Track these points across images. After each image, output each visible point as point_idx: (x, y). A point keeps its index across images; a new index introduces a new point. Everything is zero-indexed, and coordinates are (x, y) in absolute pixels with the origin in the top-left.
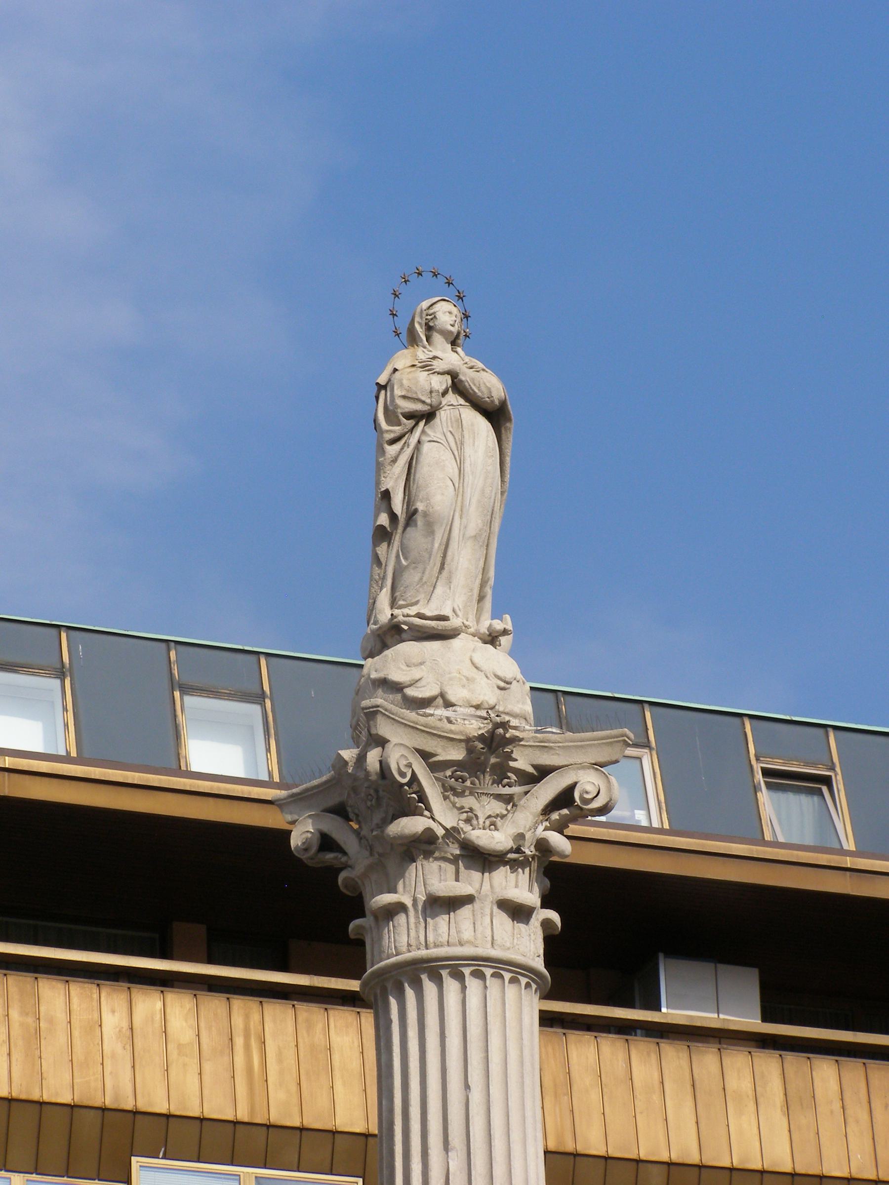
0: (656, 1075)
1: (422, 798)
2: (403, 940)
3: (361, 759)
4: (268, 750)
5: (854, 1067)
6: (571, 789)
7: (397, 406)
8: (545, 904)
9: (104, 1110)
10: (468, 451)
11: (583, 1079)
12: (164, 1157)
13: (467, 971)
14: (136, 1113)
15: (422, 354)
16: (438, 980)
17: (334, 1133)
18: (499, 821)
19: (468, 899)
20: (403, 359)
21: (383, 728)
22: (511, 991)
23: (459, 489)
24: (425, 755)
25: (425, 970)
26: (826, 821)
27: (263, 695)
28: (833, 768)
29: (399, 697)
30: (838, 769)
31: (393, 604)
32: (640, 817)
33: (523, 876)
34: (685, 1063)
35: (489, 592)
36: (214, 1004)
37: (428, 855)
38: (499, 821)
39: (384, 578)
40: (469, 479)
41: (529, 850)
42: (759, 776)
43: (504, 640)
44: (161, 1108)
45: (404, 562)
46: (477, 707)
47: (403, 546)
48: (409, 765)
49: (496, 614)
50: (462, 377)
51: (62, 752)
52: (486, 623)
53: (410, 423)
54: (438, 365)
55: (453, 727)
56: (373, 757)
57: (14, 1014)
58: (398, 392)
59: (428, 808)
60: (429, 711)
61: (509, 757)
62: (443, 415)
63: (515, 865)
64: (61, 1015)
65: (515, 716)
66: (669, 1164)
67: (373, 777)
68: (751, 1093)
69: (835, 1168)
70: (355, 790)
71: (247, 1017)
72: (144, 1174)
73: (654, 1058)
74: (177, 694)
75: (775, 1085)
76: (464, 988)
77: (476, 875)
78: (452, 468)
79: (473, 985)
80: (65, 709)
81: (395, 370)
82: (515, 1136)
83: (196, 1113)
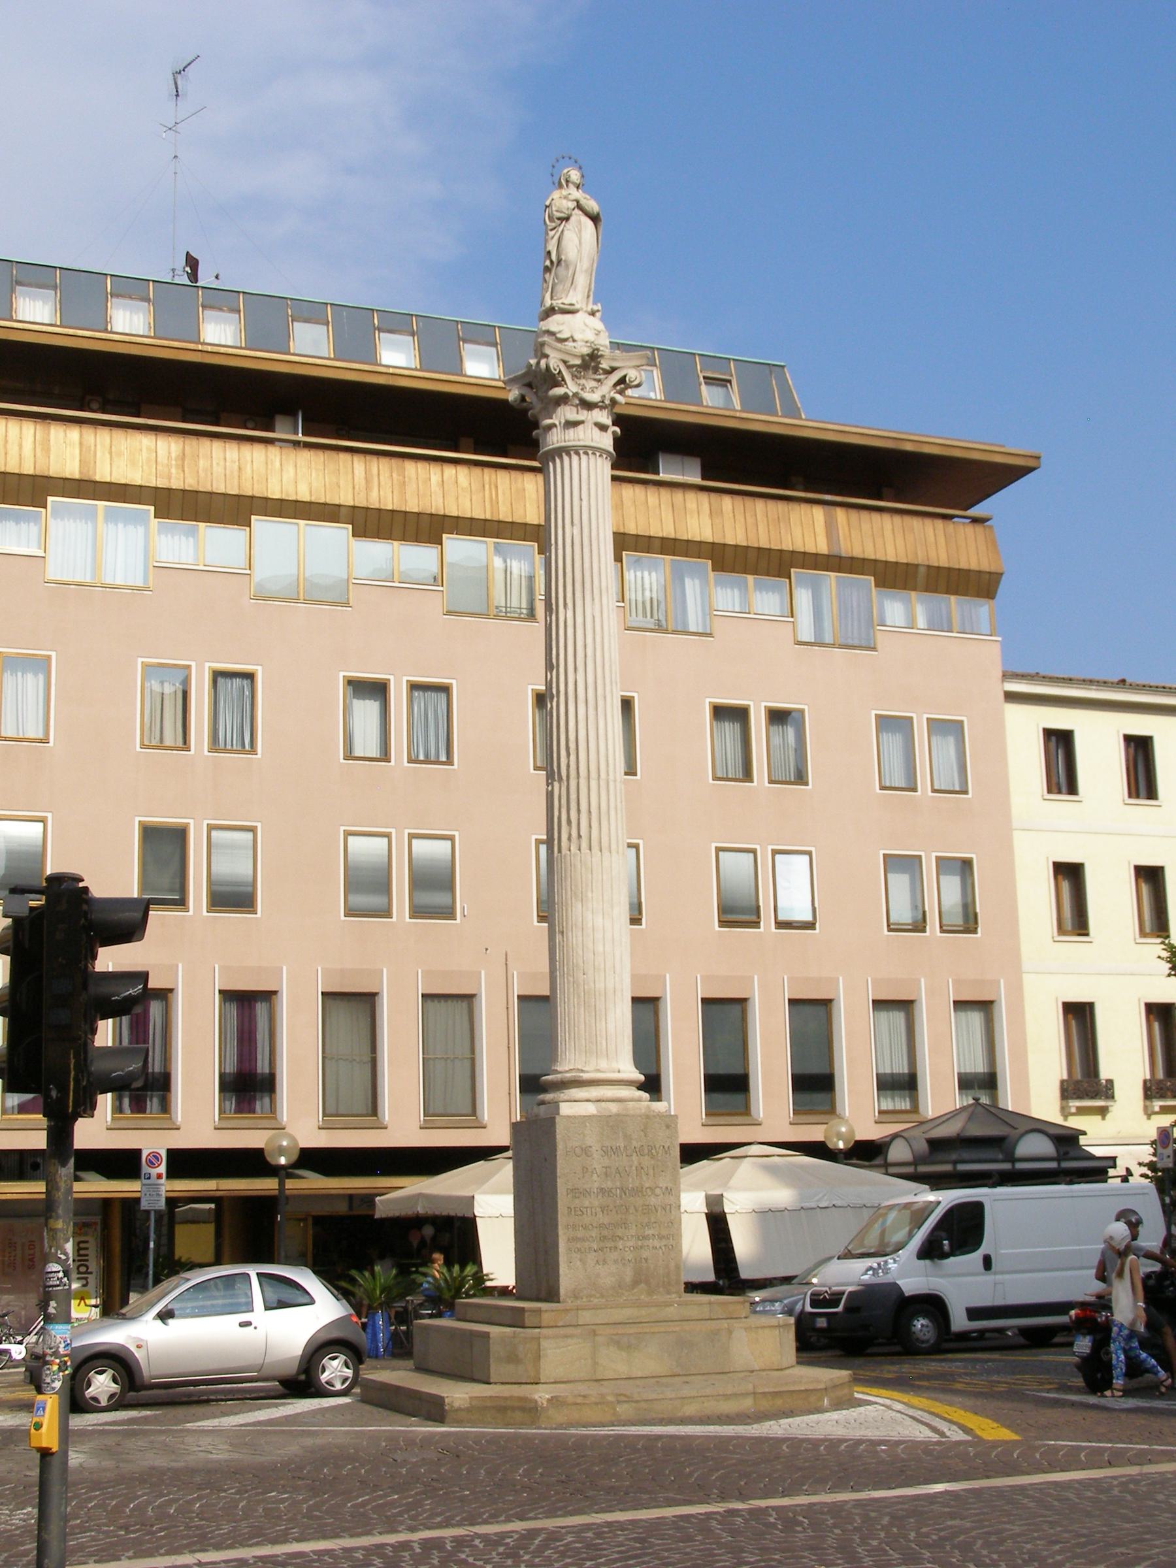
0: (657, 501)
1: (563, 380)
2: (555, 439)
3: (538, 363)
4: (499, 366)
5: (739, 500)
6: (625, 377)
7: (553, 215)
8: (614, 424)
9: (432, 515)
10: (583, 233)
11: (627, 502)
12: (457, 534)
13: (581, 452)
14: (445, 516)
15: (564, 192)
16: (569, 455)
17: (526, 524)
18: (595, 390)
19: (582, 422)
20: (556, 195)
21: (547, 350)
22: (599, 460)
23: (579, 251)
24: (565, 362)
25: (564, 451)
26: (728, 398)
27: (497, 344)
28: (732, 376)
29: (554, 338)
30: (734, 376)
31: (552, 298)
32: (652, 395)
33: (605, 412)
34: (669, 496)
35: (591, 293)
36: (477, 471)
37: (566, 403)
38: (595, 390)
39: (548, 288)
40: (584, 245)
41: (607, 402)
42: (702, 379)
43: (598, 315)
44: (455, 514)
45: (556, 281)
46: (587, 342)
47: (555, 273)
48: (558, 366)
49: (595, 303)
50: (581, 202)
51: (414, 367)
52: (590, 307)
53: (559, 222)
54: (571, 197)
55: (576, 350)
56: (543, 363)
57: (394, 475)
58: (554, 209)
59: (566, 384)
60: (566, 343)
61: (599, 363)
62: (573, 219)
63: (602, 408)
64: (413, 476)
65: (602, 346)
66: (663, 538)
67: (543, 371)
68: (696, 510)
69: (730, 541)
70: (536, 377)
71: (490, 477)
72: (448, 541)
73: (657, 494)
74: (461, 343)
75: (706, 506)
76: (580, 459)
77: (585, 412)
78: (576, 241)
79: (584, 457)
80: (415, 349)
81: (553, 199)
82: (601, 520)
83: (469, 516)
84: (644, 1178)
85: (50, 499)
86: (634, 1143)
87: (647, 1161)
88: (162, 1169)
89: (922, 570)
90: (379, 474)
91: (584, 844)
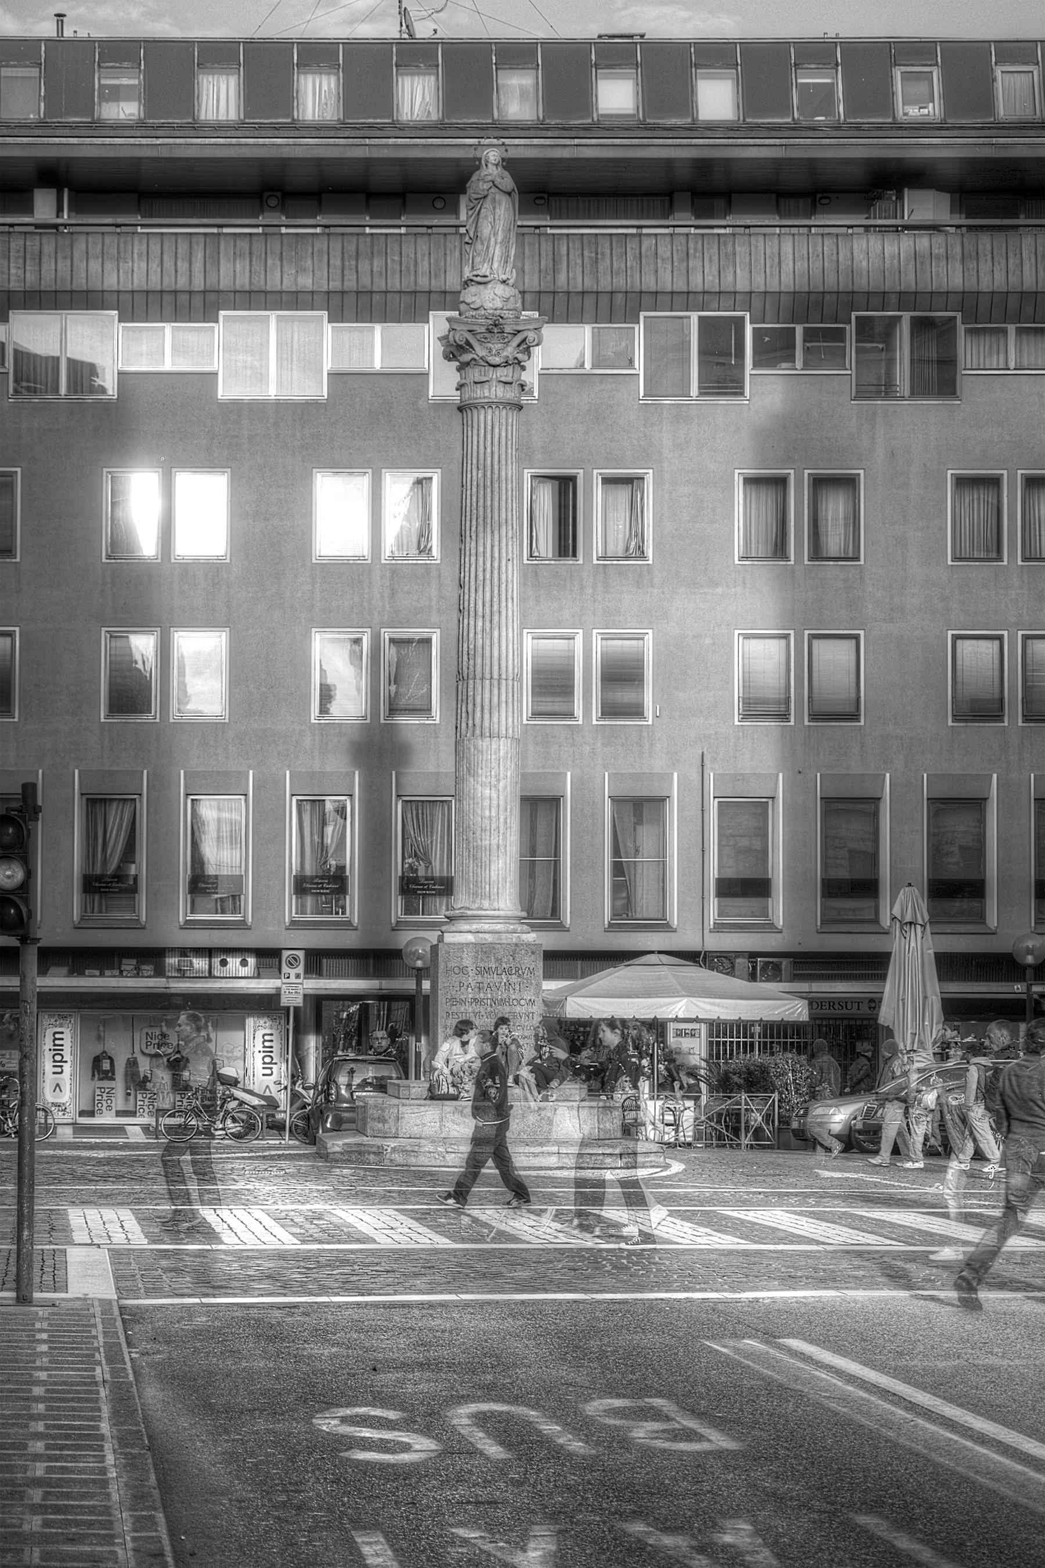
84: (512, 992)
85: (222, 313)
86: (504, 965)
87: (514, 979)
88: (300, 970)
90: (568, 254)
91: (478, 732)
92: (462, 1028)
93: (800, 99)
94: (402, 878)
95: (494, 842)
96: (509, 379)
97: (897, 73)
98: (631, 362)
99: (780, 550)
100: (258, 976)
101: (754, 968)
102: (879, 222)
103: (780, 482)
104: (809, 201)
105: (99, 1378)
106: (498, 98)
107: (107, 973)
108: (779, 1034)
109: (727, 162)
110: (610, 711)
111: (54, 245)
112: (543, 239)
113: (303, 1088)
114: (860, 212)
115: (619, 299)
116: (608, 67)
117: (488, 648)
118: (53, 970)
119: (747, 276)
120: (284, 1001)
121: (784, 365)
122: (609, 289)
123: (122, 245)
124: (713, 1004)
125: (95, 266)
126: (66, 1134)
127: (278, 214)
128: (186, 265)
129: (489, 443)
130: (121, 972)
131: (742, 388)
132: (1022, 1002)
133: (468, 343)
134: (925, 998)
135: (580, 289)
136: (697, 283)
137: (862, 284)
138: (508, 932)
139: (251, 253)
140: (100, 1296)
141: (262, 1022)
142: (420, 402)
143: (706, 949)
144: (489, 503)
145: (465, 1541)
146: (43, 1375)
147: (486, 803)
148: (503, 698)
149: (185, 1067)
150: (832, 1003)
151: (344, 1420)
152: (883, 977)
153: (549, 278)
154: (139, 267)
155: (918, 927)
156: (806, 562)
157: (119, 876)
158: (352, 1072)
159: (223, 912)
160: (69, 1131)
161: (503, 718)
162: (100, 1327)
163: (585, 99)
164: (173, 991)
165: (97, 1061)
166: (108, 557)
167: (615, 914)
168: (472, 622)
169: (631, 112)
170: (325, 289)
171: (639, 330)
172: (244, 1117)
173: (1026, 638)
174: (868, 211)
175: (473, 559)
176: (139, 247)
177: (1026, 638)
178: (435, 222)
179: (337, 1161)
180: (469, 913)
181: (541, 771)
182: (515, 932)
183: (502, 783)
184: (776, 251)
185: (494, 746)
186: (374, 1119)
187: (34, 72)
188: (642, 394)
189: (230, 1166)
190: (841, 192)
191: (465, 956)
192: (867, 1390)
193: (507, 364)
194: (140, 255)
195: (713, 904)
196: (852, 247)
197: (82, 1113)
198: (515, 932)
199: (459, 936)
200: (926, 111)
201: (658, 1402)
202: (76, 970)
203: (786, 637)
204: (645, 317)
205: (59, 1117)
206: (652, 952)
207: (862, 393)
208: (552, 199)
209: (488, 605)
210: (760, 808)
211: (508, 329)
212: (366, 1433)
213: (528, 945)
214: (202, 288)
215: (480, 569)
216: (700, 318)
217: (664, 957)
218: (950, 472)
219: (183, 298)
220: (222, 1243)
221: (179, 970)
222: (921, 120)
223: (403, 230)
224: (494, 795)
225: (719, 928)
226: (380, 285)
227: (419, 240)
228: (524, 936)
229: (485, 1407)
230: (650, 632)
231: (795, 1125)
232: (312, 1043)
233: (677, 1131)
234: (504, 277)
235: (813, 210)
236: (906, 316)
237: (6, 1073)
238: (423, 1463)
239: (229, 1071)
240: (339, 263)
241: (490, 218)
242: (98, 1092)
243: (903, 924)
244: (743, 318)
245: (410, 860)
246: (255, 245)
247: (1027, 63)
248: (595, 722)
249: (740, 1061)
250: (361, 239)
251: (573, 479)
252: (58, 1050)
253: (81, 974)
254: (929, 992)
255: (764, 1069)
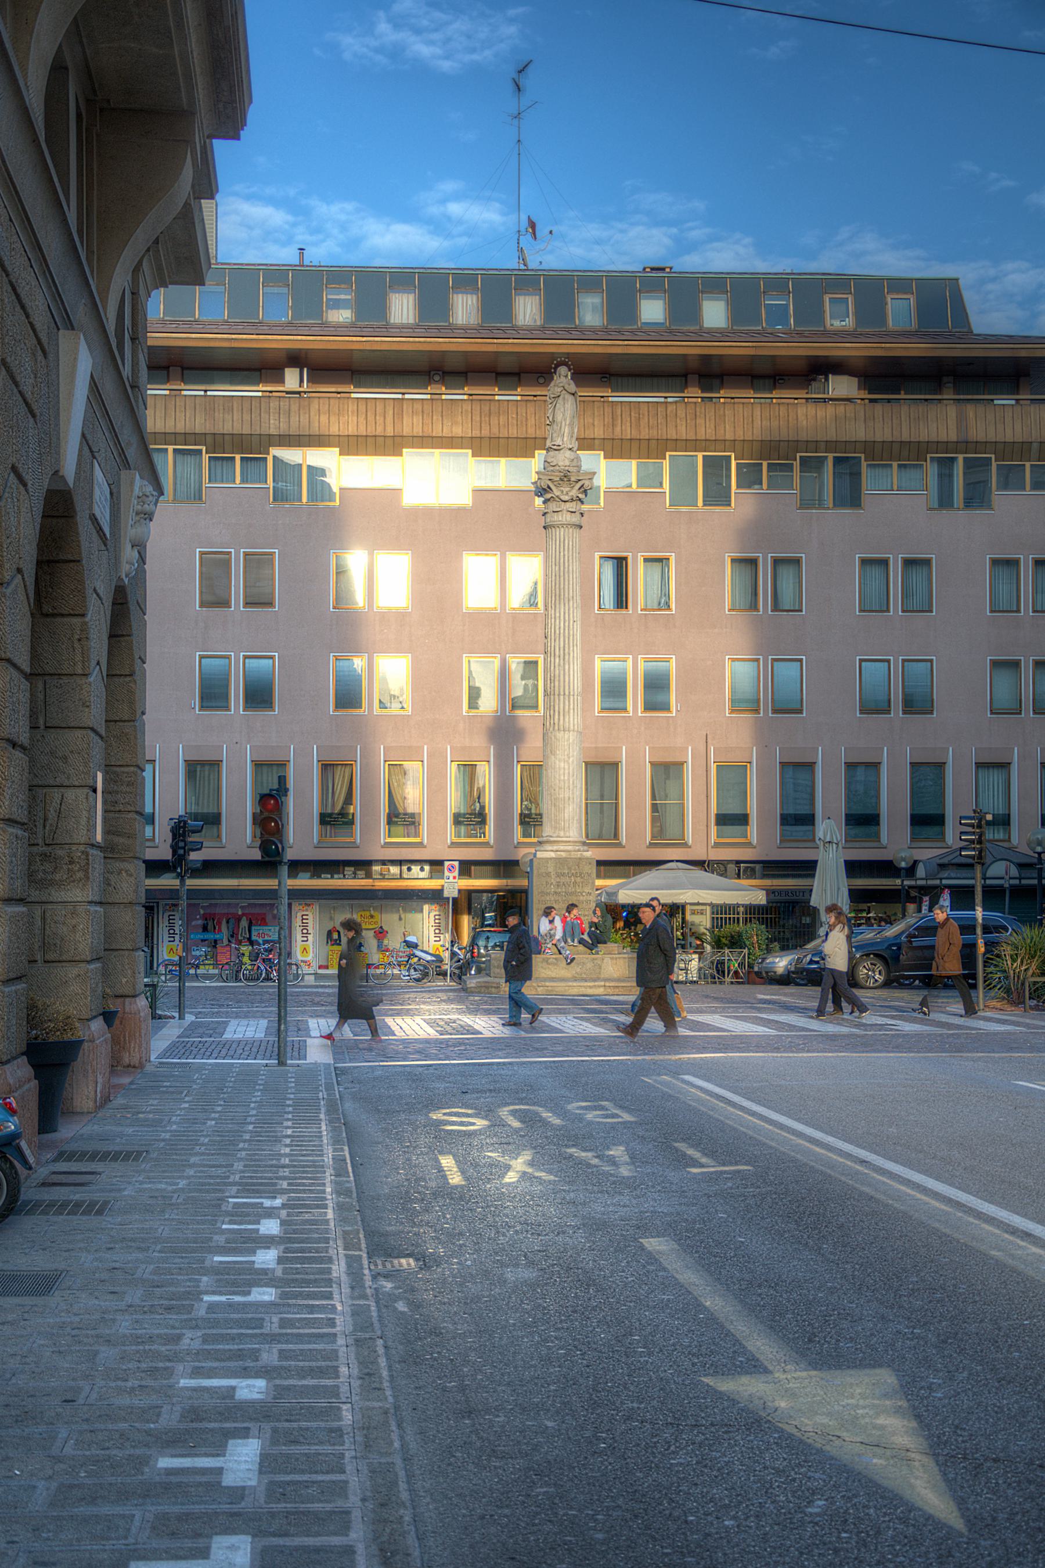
87: (578, 880)
88: (456, 873)
89: (1035, 446)
91: (556, 728)
92: (547, 912)
93: (766, 313)
94: (521, 814)
95: (567, 796)
96: (573, 510)
97: (827, 298)
98: (661, 484)
99: (754, 606)
100: (431, 878)
101: (739, 870)
102: (814, 396)
103: (753, 562)
104: (772, 381)
105: (321, 1097)
106: (579, 312)
107: (336, 876)
108: (759, 912)
109: (721, 357)
110: (649, 707)
111: (297, 405)
112: (606, 404)
113: (459, 949)
114: (802, 388)
115: (653, 444)
116: (647, 292)
117: (562, 676)
118: (301, 875)
119: (732, 429)
120: (446, 894)
121: (756, 487)
122: (647, 437)
123: (341, 406)
124: (708, 894)
125: (324, 419)
126: (310, 980)
127: (440, 386)
128: (382, 419)
129: (562, 549)
130: (344, 876)
131: (730, 501)
132: (899, 890)
133: (549, 487)
134: (839, 889)
135: (629, 437)
136: (701, 435)
137: (803, 437)
138: (575, 851)
139: (423, 412)
140: (324, 1062)
141: (433, 907)
142: (530, 509)
143: (710, 859)
144: (562, 586)
145: (489, 1157)
146: (292, 1096)
147: (562, 772)
148: (572, 707)
149: (385, 937)
150: (780, 892)
151: (444, 1114)
152: (813, 876)
153: (610, 430)
154: (352, 420)
155: (834, 845)
156: (770, 613)
157: (343, 814)
158: (488, 938)
159: (408, 837)
160: (312, 978)
161: (572, 719)
162: (323, 1076)
163: (632, 311)
164: (377, 888)
165: (329, 934)
166: (334, 608)
167: (653, 837)
168: (552, 660)
169: (662, 321)
170: (470, 435)
171: (666, 464)
172: (422, 968)
173: (904, 661)
174: (807, 388)
175: (553, 620)
176: (352, 407)
177: (904, 661)
178: (539, 393)
179: (472, 992)
180: (552, 839)
181: (606, 745)
182: (579, 850)
183: (571, 759)
184: (750, 414)
185: (566, 736)
186: (494, 967)
187: (285, 290)
188: (668, 505)
189: (408, 996)
190: (792, 375)
191: (549, 865)
192: (711, 1096)
193: (572, 500)
194: (353, 412)
195: (713, 829)
196: (797, 412)
197: (320, 967)
198: (579, 850)
199: (546, 854)
200: (843, 323)
201: (603, 1103)
202: (316, 875)
203: (758, 660)
204: (670, 456)
205: (306, 969)
206: (672, 861)
207: (805, 504)
208: (612, 378)
209: (562, 649)
210: (741, 770)
211: (573, 479)
212: (454, 1119)
213: (587, 859)
214: (392, 434)
215: (557, 627)
216: (703, 456)
217: (679, 864)
218: (857, 556)
219: (380, 440)
220: (395, 1035)
221: (381, 874)
222: (841, 329)
223: (519, 398)
224: (566, 767)
225: (717, 845)
226: (504, 433)
227: (529, 404)
228: (585, 854)
229: (517, 1107)
230: (674, 657)
231: (756, 969)
232: (466, 921)
233: (686, 973)
234: (571, 447)
235: (774, 387)
236: (831, 456)
237: (272, 941)
238: (480, 1130)
239: (411, 939)
240: (478, 419)
241: (562, 410)
242: (330, 953)
243: (825, 843)
244: (730, 457)
245: (526, 803)
246: (425, 407)
247: (906, 293)
248: (640, 715)
249: (729, 929)
250: (493, 403)
251: (625, 559)
252: (305, 926)
253: (319, 877)
254: (841, 886)
255: (740, 934)
